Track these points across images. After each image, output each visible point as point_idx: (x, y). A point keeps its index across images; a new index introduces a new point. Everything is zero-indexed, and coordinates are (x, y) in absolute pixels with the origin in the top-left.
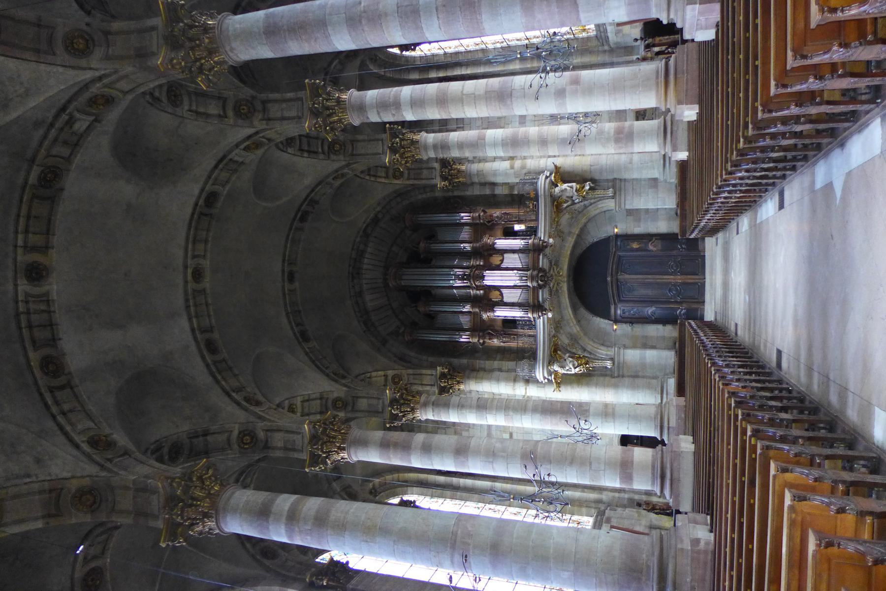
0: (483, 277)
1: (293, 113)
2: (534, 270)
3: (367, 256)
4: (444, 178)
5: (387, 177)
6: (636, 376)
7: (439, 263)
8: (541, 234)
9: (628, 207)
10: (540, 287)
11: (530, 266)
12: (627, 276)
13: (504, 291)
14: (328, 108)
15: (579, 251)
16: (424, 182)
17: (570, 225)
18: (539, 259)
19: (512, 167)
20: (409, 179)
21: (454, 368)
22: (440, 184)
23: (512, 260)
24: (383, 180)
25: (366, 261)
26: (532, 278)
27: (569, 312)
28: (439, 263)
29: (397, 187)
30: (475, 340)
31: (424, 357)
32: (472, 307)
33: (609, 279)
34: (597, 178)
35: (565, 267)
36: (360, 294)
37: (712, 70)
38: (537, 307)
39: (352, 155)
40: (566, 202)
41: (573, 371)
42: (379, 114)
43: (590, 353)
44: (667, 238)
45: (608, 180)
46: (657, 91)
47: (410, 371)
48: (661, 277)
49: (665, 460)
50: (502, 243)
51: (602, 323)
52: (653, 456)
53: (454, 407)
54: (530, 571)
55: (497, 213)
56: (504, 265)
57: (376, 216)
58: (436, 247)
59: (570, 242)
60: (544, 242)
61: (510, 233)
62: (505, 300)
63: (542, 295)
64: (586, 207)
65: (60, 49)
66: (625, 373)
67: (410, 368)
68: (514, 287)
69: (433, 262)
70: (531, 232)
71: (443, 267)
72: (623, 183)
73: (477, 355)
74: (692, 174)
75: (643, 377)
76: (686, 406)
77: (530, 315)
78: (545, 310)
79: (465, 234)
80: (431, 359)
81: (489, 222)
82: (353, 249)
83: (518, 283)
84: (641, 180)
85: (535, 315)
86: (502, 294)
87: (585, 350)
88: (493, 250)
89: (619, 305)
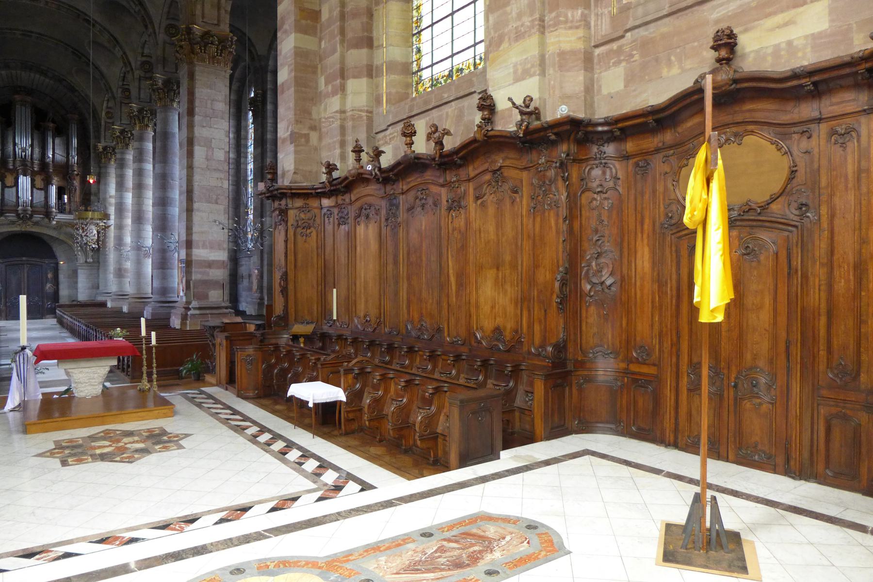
0: (25, 175)
1: (142, 96)
4: (105, 148)
5: (107, 107)
7: (36, 143)
8: (60, 216)
9: (79, 271)
10: (18, 215)
12: (26, 271)
13: (14, 189)
14: (143, 118)
15: (45, 238)
16: (103, 133)
17: (66, 234)
19: (111, 197)
20: (106, 122)
22: (100, 146)
23: (39, 196)
24: (105, 105)
25: (37, 76)
26: (25, 211)
28: (35, 136)
33: (24, 258)
35: (33, 230)
39: (121, 103)
44: (56, 296)
45: (98, 258)
50: (53, 190)
54: (425, 472)
55: (76, 183)
56: (35, 190)
58: (50, 134)
59: (53, 233)
61: (60, 192)
62: (6, 190)
65: (169, 22)
68: (18, 197)
69: (36, 131)
70: (61, 209)
74: (102, 310)
79: (60, 157)
86: (11, 187)
88: (48, 183)
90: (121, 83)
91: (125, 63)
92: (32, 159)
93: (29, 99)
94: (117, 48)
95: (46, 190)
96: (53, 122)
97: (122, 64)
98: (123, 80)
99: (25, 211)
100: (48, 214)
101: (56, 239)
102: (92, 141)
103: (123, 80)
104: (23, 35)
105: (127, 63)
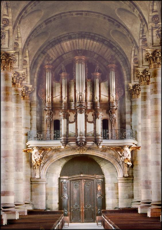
0: (81, 113)
2: (86, 139)
3: (92, 41)
5: (135, 55)
6: (31, 191)
10: (77, 142)
11: (88, 138)
13: (74, 123)
14: (156, 58)
15: (96, 159)
18: (91, 141)
21: (31, 93)
22: (131, 85)
23: (90, 128)
25: (89, 41)
26: (81, 139)
27: (64, 155)
29: (129, 60)
30: (47, 105)
31: (36, 76)
32: (65, 104)
33: (82, 175)
34: (134, 168)
36: (70, 38)
37: (145, 221)
38: (66, 142)
40: (121, 153)
41: (33, 159)
42: (153, 83)
43: (42, 167)
46: (157, 202)
47: (28, 69)
48: (98, 82)
49: (11, 208)
50: (99, 122)
51: (58, 170)
52: (12, 204)
53: (17, 106)
56: (87, 123)
57: (114, 47)
59: (100, 155)
60: (100, 144)
62: (70, 124)
63: (73, 144)
64: (119, 163)
66: (33, 185)
67: (30, 69)
68: (77, 129)
71: (86, 86)
72: (131, 181)
73: (39, 105)
75: (31, 194)
76: (7, 214)
77: (62, 138)
78: (65, 145)
79: (104, 97)
80: (35, 80)
81: (111, 111)
82: (95, 34)
83: (79, 132)
84: (133, 190)
85: (62, 140)
86: (72, 122)
87: (44, 164)
89: (68, 181)
90: (141, 36)
91: (141, 20)
92: (86, 100)
93: (83, 58)
94: (136, 10)
95: (94, 122)
96: (99, 71)
97: (140, 22)
98: (143, 33)
99: (81, 139)
100: (96, 141)
101: (103, 159)
102: (126, 82)
103: (143, 33)
104: (77, 14)
105: (143, 20)
